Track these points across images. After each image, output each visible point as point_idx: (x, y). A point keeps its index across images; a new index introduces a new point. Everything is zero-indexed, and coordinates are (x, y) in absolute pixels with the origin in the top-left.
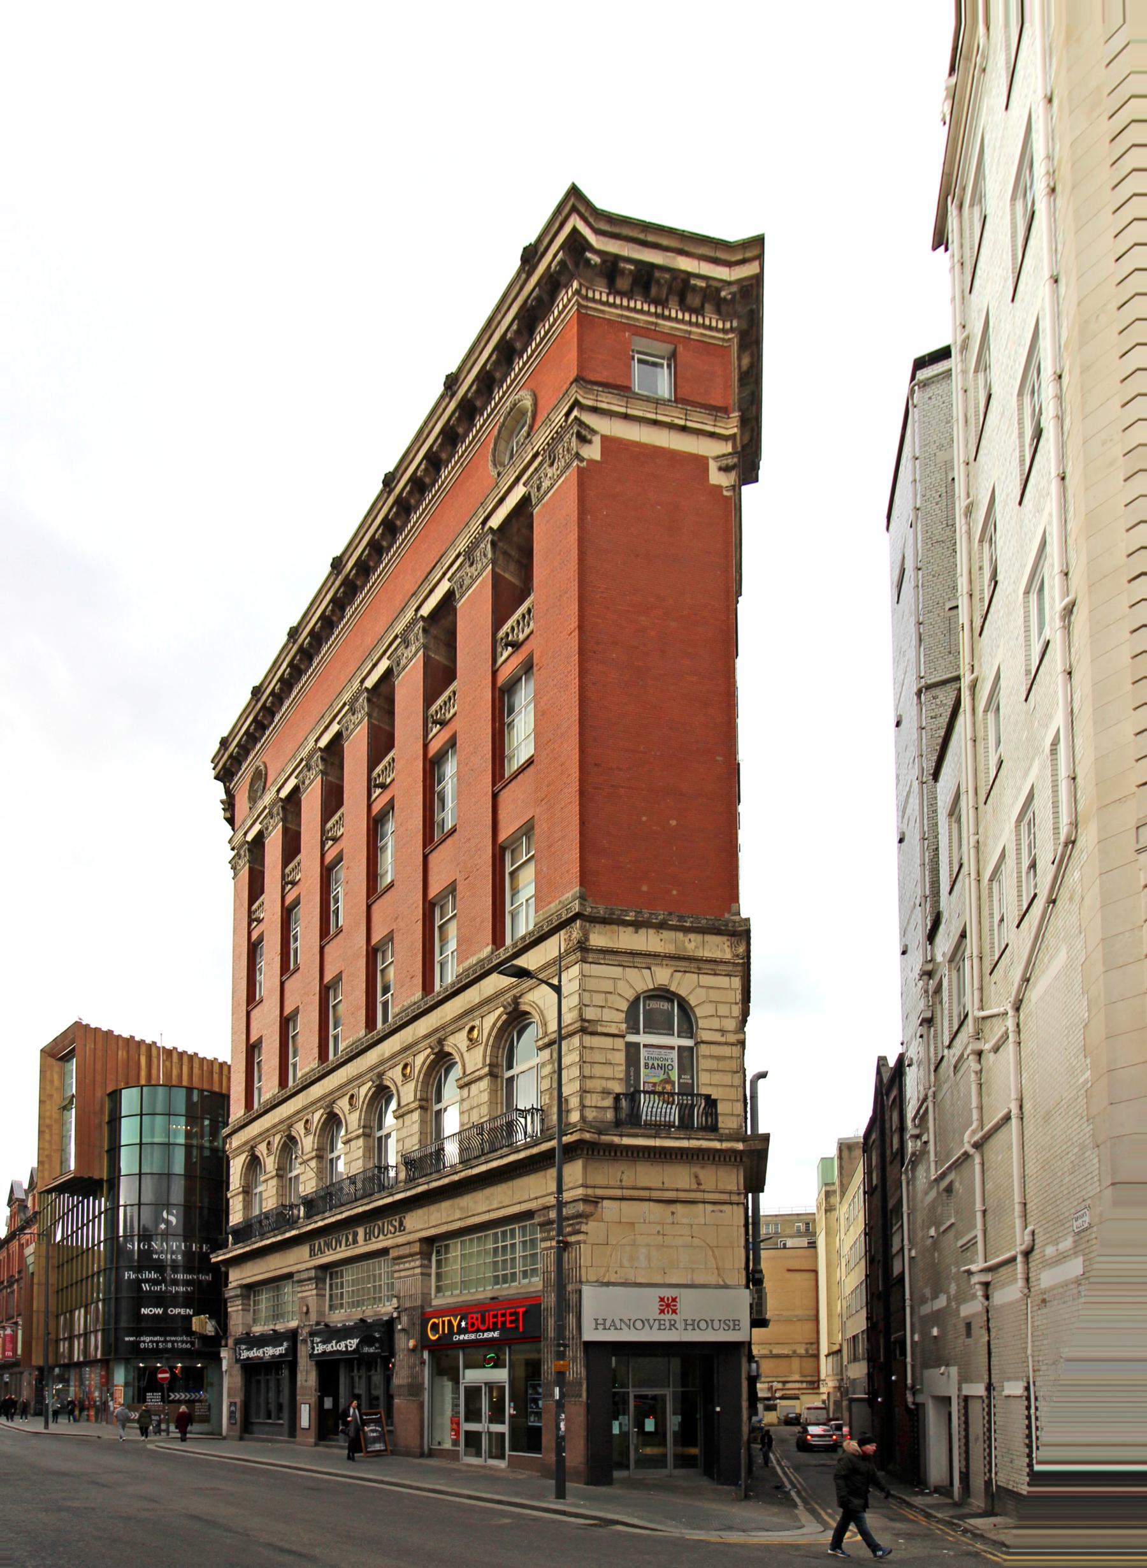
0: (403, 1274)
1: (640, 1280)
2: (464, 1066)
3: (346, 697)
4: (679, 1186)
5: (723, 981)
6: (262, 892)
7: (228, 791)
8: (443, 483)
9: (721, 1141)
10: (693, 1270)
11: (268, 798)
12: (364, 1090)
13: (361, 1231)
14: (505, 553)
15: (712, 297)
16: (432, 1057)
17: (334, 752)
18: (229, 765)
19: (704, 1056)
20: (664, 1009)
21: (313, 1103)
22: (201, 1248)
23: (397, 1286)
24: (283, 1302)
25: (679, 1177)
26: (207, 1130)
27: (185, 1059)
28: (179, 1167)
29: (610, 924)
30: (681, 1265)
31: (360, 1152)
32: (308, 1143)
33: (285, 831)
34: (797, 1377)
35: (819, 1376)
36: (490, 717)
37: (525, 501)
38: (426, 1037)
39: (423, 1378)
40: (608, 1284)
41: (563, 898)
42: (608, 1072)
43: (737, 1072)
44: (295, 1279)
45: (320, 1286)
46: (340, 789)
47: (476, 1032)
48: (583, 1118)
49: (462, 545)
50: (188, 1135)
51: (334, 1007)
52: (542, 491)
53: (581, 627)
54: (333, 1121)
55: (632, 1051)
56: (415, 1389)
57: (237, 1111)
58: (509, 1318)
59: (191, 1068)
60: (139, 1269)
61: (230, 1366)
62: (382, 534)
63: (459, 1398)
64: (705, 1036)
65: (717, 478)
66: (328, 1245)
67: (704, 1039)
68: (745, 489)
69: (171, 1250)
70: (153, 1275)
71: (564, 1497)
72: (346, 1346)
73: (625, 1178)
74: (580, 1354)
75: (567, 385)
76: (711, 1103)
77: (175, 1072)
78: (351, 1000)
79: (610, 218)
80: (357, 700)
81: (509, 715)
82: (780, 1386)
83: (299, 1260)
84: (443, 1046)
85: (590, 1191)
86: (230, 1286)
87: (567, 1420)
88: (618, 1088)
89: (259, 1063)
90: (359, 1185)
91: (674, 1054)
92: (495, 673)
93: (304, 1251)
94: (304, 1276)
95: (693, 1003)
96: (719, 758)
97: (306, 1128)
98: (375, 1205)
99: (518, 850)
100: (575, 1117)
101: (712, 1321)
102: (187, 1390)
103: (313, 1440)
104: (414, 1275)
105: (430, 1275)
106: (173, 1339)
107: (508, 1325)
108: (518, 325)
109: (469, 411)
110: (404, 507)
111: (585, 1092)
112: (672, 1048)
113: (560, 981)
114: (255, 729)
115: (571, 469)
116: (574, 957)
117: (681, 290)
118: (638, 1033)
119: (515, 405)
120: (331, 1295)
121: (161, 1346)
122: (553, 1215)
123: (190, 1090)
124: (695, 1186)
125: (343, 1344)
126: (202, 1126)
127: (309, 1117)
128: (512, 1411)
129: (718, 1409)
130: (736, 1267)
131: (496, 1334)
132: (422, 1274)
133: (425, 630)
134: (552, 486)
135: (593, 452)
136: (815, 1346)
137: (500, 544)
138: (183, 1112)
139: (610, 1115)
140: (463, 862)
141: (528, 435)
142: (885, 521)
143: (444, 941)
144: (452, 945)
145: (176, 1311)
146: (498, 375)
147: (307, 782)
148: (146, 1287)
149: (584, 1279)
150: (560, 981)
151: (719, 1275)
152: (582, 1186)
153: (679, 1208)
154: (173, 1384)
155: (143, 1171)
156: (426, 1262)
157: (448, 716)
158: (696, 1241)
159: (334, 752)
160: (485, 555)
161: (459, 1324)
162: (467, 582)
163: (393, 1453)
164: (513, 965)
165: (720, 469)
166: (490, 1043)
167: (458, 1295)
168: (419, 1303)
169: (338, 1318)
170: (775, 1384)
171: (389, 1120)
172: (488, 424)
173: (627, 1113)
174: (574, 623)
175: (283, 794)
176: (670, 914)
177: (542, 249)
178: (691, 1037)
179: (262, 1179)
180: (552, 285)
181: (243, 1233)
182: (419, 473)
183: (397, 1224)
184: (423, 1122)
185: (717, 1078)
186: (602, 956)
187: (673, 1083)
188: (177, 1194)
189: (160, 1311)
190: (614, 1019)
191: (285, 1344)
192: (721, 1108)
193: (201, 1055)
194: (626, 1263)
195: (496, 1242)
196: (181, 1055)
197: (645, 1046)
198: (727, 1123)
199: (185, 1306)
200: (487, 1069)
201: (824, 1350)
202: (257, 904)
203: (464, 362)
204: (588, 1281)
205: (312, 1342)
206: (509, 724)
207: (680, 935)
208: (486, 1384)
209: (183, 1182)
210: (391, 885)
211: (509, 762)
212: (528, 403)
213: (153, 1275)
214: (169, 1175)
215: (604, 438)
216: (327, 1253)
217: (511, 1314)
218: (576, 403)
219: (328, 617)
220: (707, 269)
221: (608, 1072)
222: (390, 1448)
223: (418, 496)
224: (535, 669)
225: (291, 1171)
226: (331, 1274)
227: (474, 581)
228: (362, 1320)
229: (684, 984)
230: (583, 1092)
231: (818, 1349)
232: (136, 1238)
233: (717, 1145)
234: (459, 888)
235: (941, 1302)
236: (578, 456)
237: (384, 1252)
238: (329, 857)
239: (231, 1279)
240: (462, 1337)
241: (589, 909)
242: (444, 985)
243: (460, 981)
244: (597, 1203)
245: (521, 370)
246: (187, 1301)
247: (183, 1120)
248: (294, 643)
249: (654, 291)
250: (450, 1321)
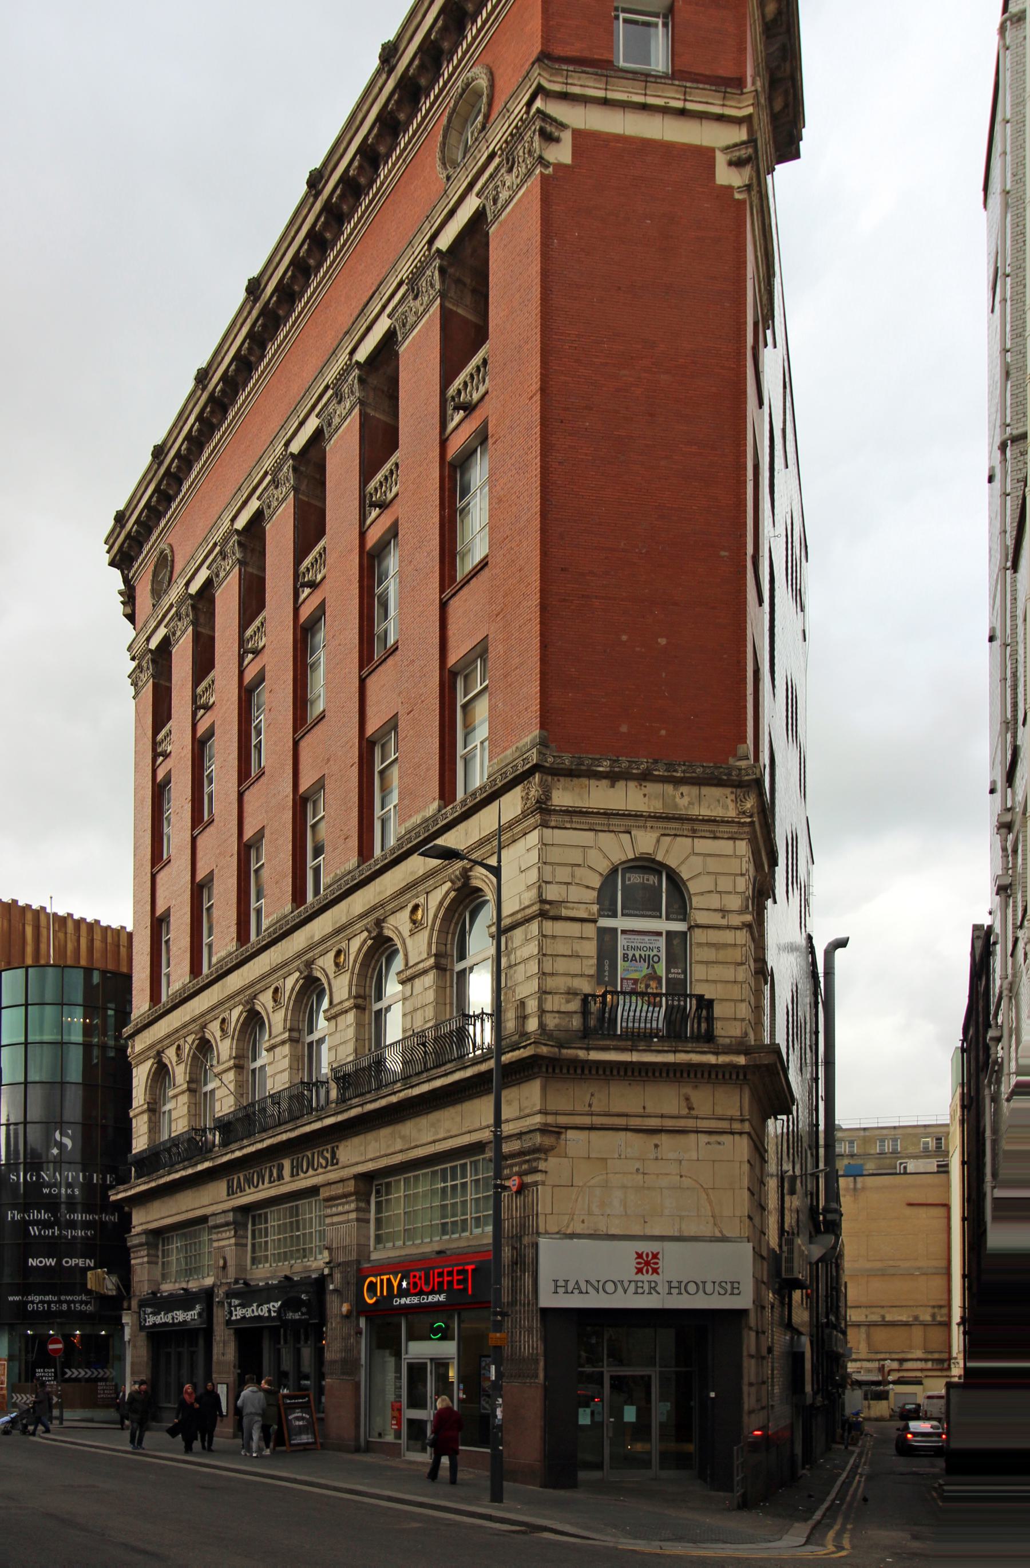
0: (335, 1219)
1: (613, 1231)
2: (406, 955)
3: (268, 464)
4: (664, 1112)
5: (725, 846)
6: (169, 718)
7: (126, 581)
8: (382, 184)
9: (716, 1054)
10: (681, 1218)
11: (174, 594)
12: (290, 982)
13: (287, 1164)
14: (458, 281)
16: (370, 942)
17: (253, 536)
19: (700, 945)
21: (231, 997)
22: (104, 1179)
23: (328, 1235)
24: (198, 1251)
25: (664, 1101)
26: (111, 1021)
27: (84, 929)
28: (75, 1073)
29: (579, 776)
30: (667, 1212)
31: (286, 1063)
32: (225, 1049)
33: (197, 637)
34: (919, 1354)
35: (950, 1352)
36: (437, 502)
37: (479, 218)
38: (362, 916)
39: (359, 1353)
40: (572, 1236)
41: (520, 744)
42: (574, 966)
43: (742, 964)
44: (211, 1223)
45: (240, 1233)
46: (262, 581)
47: (420, 912)
48: (542, 1025)
49: (404, 270)
50: (87, 1030)
51: (257, 871)
52: (499, 205)
53: (543, 390)
55: (607, 939)
56: (349, 1366)
57: (140, 1005)
58: (456, 1278)
59: (91, 941)
60: (25, 1208)
61: (133, 1335)
62: (309, 250)
63: (400, 1378)
64: (701, 918)
65: (726, 176)
66: (249, 1181)
67: (700, 921)
69: (66, 1181)
70: (44, 1216)
71: (501, 1501)
72: (173, 1318)
73: (595, 1101)
74: (536, 1324)
75: (527, 66)
76: (705, 1004)
77: (70, 946)
78: (275, 861)
80: (280, 469)
81: (462, 498)
82: (895, 1365)
83: (214, 1200)
84: (382, 928)
85: (550, 1119)
86: (134, 1231)
87: (505, 1405)
88: (586, 987)
89: (209, 909)
90: (284, 1105)
91: (662, 942)
92: (443, 443)
93: (218, 1189)
94: (220, 1220)
95: (685, 876)
96: (723, 553)
97: (222, 1030)
99: (472, 676)
100: (532, 1025)
101: (704, 1283)
102: (88, 1365)
103: (231, 1430)
104: (348, 1221)
105: (368, 1221)
106: (69, 1298)
107: (456, 1286)
108: (444, 21)
109: (411, 92)
110: (335, 216)
111: (545, 992)
112: (659, 934)
113: (499, 861)
114: (158, 501)
115: (533, 177)
116: (532, 820)
118: (614, 915)
119: (468, 85)
120: (253, 1245)
121: (53, 1307)
123: (88, 971)
124: (685, 1112)
125: (265, 1307)
126: (105, 1017)
127: (226, 1015)
128: (462, 1396)
129: (712, 1395)
130: (738, 1214)
131: (442, 1298)
132: (358, 1220)
133: (361, 380)
134: (511, 198)
135: (562, 153)
136: (944, 1311)
137: (451, 270)
138: (80, 1001)
139: (576, 1022)
140: (405, 689)
141: (484, 127)
142: (982, 194)
143: (469, 729)
144: (482, 732)
145: (73, 1262)
146: (446, 45)
147: (222, 574)
148: (34, 1231)
149: (541, 1230)
150: (499, 861)
151: (715, 1224)
152: (540, 1112)
153: (664, 1139)
154: (70, 1356)
155: (29, 1079)
156: (363, 1205)
157: (390, 496)
158: (687, 1182)
159: (253, 536)
160: (432, 286)
161: (400, 1285)
162: (412, 319)
163: (323, 1446)
164: (435, 845)
165: (731, 164)
166: (437, 927)
167: (401, 1248)
168: (354, 1257)
169: (263, 1274)
170: (888, 1362)
171: (393, 988)
172: (435, 109)
173: (597, 1022)
174: (536, 386)
175: (193, 589)
176: (656, 762)
177: (169, 445)
178: (684, 920)
179: (171, 1093)
182: (351, 173)
183: (328, 1156)
184: (359, 1025)
185: (715, 972)
186: (567, 818)
187: (660, 979)
188: (73, 1107)
189: (51, 1262)
190: (582, 898)
191: (198, 1307)
192: (718, 1010)
193: (103, 923)
194: (595, 1210)
195: (445, 1181)
196: (79, 923)
197: (624, 932)
198: (726, 1030)
199: (84, 1256)
200: (432, 960)
202: (204, 684)
203: (404, 27)
204: (547, 1233)
205: (230, 1305)
206: (463, 509)
207: (669, 788)
208: (432, 1360)
209: (80, 1092)
210: (322, 717)
211: (311, 704)
212: (483, 82)
213: (44, 1216)
214: (62, 1083)
215: (577, 134)
216: (248, 1191)
217: (459, 1272)
218: (540, 90)
219: (354, 179)
221: (574, 966)
222: (319, 1440)
223: (351, 201)
224: (490, 441)
225: (206, 1084)
226: (254, 1217)
227: (419, 317)
228: (287, 1278)
229: (675, 852)
230: (543, 993)
231: (949, 1315)
232: (22, 1166)
233: (712, 1059)
234: (402, 725)
236: (541, 160)
237: (313, 1191)
238: (249, 675)
239: (134, 1222)
240: (403, 1301)
241: (550, 759)
242: (471, 789)
243: (400, 846)
244: (559, 1133)
245: (474, 39)
246: (87, 1249)
247: (80, 1011)
248: (203, 390)
250: (389, 1280)
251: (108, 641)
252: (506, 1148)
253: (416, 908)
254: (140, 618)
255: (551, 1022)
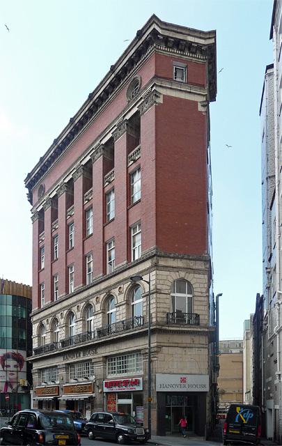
5: (202, 276)
12: (82, 304)
15: (199, 48)
17: (70, 184)
18: (33, 182)
20: (181, 284)
25: (186, 339)
31: (81, 326)
37: (137, 112)
42: (165, 306)
53: (156, 159)
54: (71, 314)
57: (35, 309)
64: (196, 294)
68: (211, 104)
76: (198, 316)
78: (75, 271)
79: (165, 24)
83: (60, 362)
93: (62, 359)
98: (85, 345)
100: (154, 320)
109: (119, 78)
117: (189, 46)
122: (147, 351)
135: (160, 100)
139: (165, 320)
153: (187, 349)
159: (70, 184)
162: (118, 135)
165: (202, 106)
172: (125, 84)
175: (51, 196)
180: (147, 44)
181: (38, 351)
193: (23, 284)
198: (203, 322)
201: (245, 392)
207: (188, 261)
220: (197, 40)
230: (157, 312)
233: (199, 330)
235: (270, 379)
249: (180, 47)
251: (25, 210)
252: (152, 350)
253: (120, 288)
254: (34, 203)
255: (159, 319)
